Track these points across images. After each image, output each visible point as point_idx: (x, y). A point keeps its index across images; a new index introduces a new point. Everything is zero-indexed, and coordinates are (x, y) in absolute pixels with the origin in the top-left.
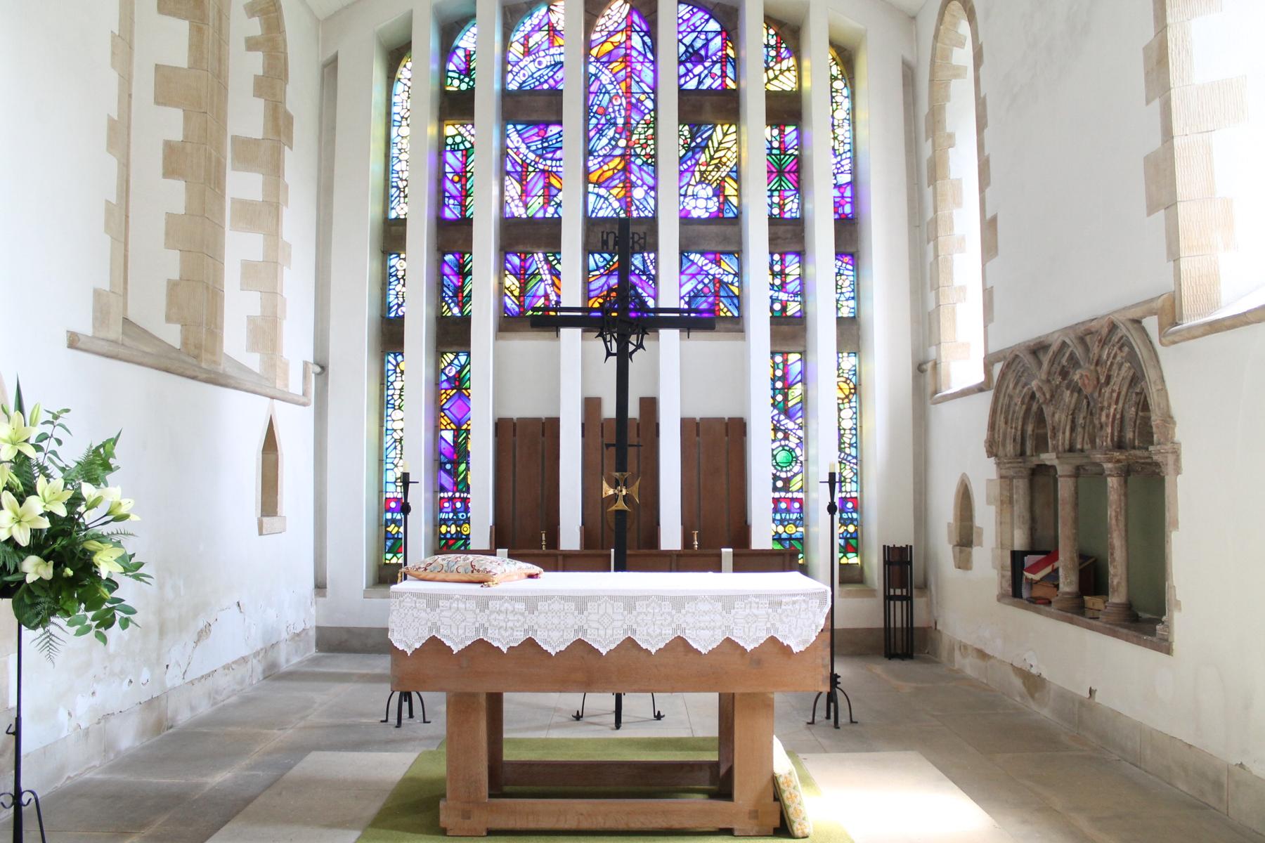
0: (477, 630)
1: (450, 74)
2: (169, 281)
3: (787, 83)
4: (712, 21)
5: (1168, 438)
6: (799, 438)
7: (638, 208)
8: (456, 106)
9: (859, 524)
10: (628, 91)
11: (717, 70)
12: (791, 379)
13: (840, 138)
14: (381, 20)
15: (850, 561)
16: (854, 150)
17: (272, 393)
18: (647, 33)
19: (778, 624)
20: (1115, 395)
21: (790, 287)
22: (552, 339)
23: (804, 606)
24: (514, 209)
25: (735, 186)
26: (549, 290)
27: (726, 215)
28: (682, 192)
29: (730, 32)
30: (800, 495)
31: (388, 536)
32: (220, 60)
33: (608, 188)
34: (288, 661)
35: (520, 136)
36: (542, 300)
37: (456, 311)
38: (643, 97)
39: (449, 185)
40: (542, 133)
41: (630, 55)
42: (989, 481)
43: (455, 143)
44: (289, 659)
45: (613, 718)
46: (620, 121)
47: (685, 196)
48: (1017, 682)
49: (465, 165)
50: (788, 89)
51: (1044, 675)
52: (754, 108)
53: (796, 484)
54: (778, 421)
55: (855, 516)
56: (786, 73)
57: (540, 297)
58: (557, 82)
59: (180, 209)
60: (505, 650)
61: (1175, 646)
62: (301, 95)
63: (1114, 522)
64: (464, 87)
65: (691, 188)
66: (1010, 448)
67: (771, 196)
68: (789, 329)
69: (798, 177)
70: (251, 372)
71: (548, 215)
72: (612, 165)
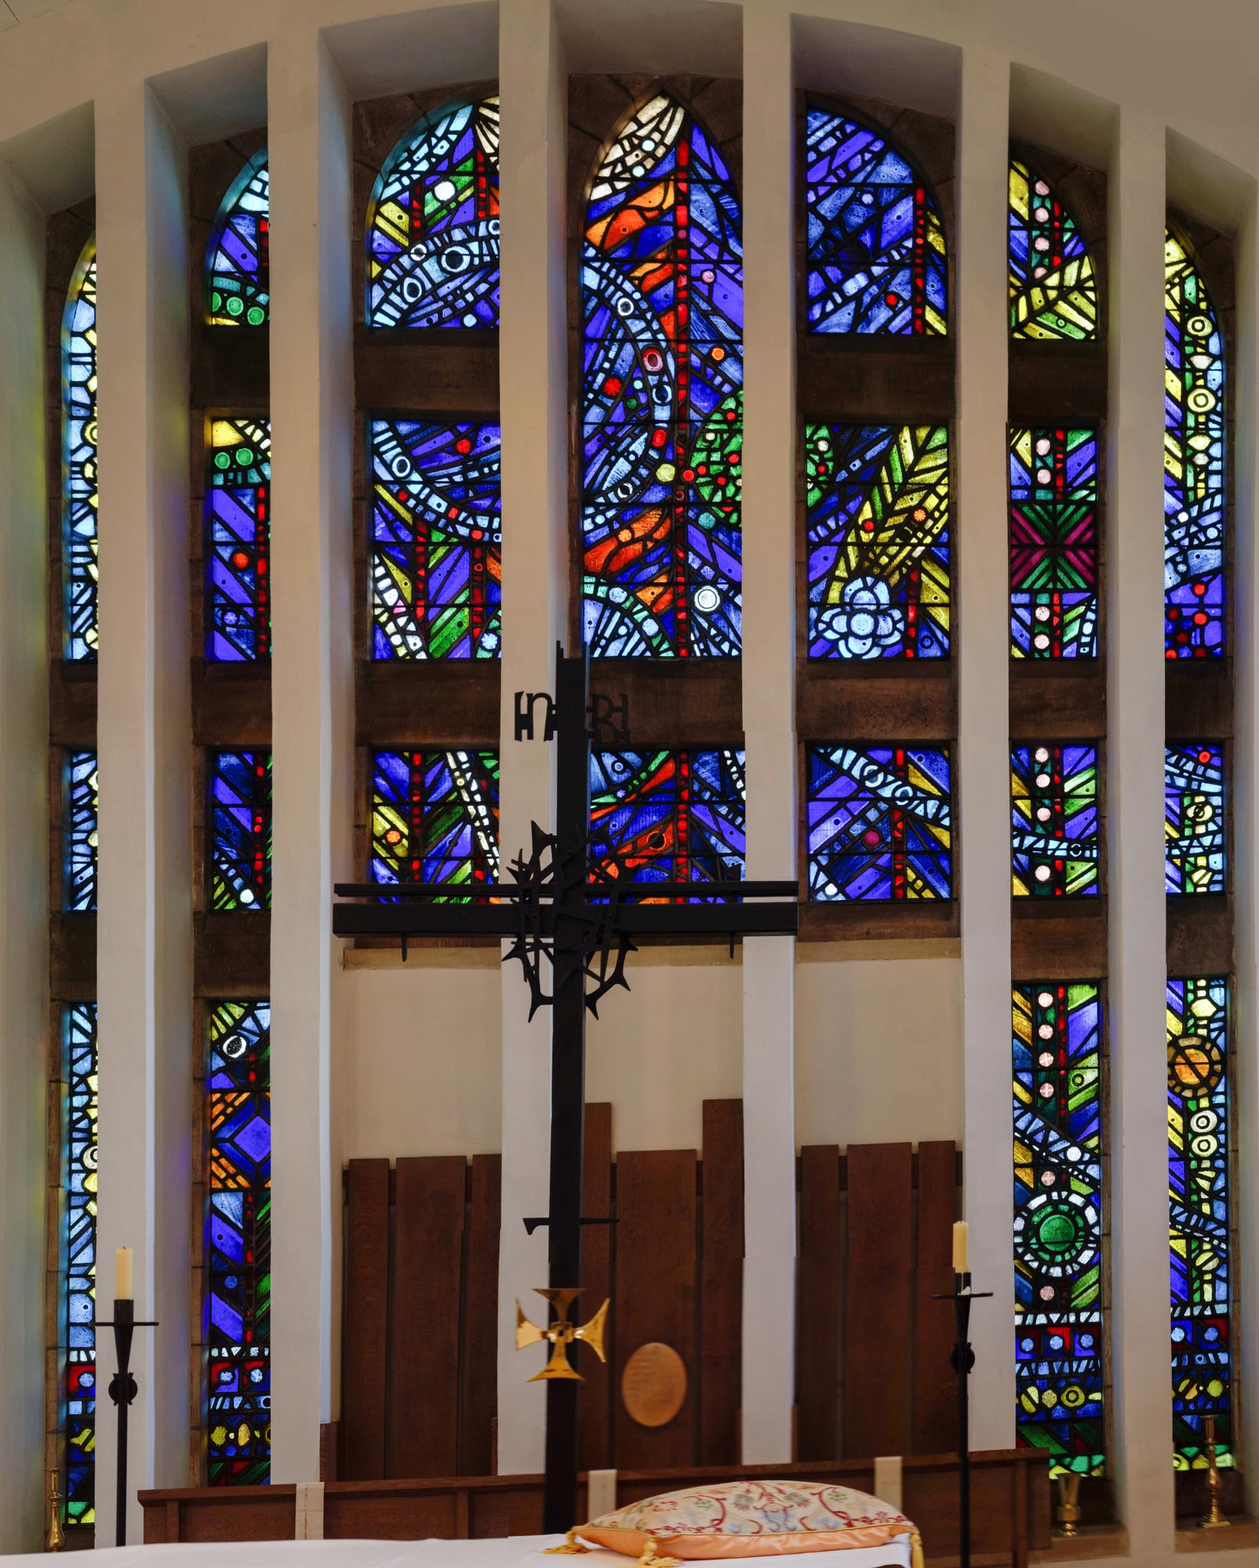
3: (1077, 319)
6: (1093, 1182)
11: (900, 285)
12: (1073, 1046)
13: (1201, 460)
21: (1073, 827)
22: (719, 961)
25: (945, 581)
28: (814, 594)
29: (935, 190)
33: (632, 587)
36: (467, 868)
39: (221, 574)
40: (464, 446)
43: (235, 467)
47: (823, 606)
54: (1046, 1145)
57: (462, 861)
68: (1060, 930)
72: (640, 529)
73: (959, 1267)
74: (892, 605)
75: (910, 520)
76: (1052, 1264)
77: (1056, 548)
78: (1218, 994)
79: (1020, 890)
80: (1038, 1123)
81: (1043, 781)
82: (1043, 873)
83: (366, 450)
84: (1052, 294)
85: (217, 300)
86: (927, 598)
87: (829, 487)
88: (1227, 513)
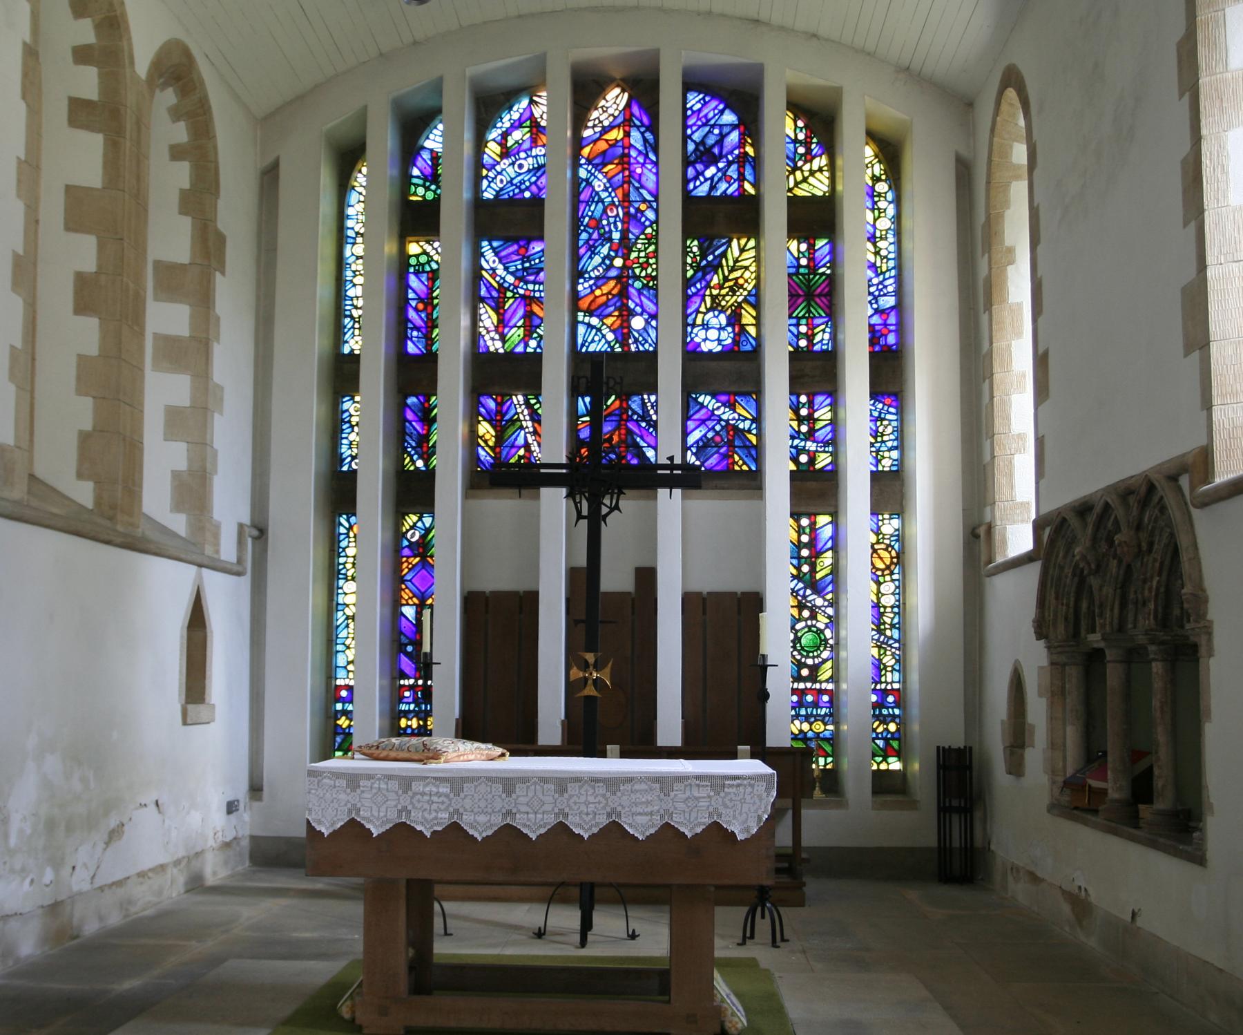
0: (400, 812)
1: (414, 181)
2: (81, 432)
3: (819, 186)
4: (727, 112)
5: (1201, 615)
6: (829, 617)
7: (636, 341)
8: (419, 219)
9: (902, 722)
10: (626, 199)
11: (733, 172)
12: (820, 545)
13: (883, 253)
14: (333, 117)
15: (891, 767)
16: (899, 267)
17: (199, 559)
18: (648, 129)
19: (721, 809)
20: (1157, 565)
23: (749, 789)
24: (489, 343)
26: (530, 439)
27: (744, 348)
29: (750, 125)
30: (830, 686)
31: (337, 730)
32: (138, 179)
33: (602, 317)
34: (215, 873)
35: (496, 254)
36: (522, 452)
37: (420, 464)
38: (643, 207)
39: (412, 314)
41: (629, 156)
42: (1040, 668)
44: (214, 870)
45: (577, 938)
46: (616, 236)
48: (1066, 908)
49: (431, 290)
50: (820, 194)
51: (1093, 898)
52: (775, 216)
53: (826, 672)
54: (804, 597)
55: (897, 712)
56: (818, 175)
57: (519, 448)
58: (540, 189)
59: (93, 349)
60: (428, 835)
61: (1209, 855)
62: (235, 212)
63: (1158, 714)
64: (430, 196)
65: (700, 316)
66: (1061, 628)
67: (797, 325)
68: (816, 489)
69: (830, 301)
70: (175, 535)
71: (529, 350)
72: (605, 289)
77: (809, 296)
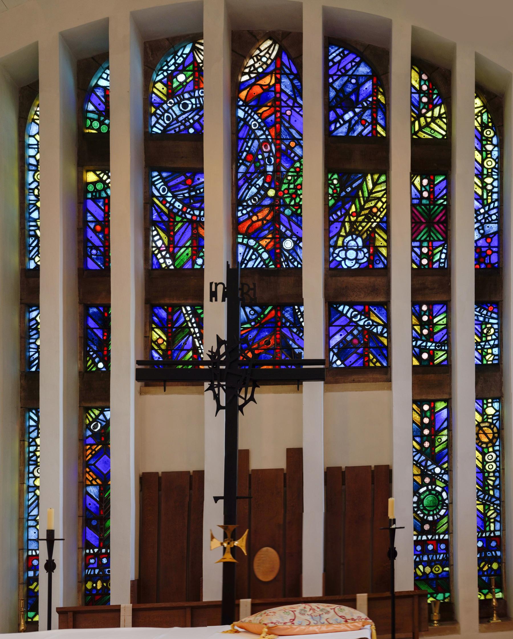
3: (439, 130)
6: (445, 482)
10: (278, 137)
11: (367, 116)
12: (437, 427)
13: (489, 187)
21: (437, 337)
22: (293, 392)
28: (332, 242)
29: (381, 77)
33: (257, 239)
36: (190, 354)
39: (90, 234)
40: (189, 182)
43: (96, 190)
47: (335, 247)
54: (426, 467)
57: (188, 351)
68: (432, 379)
72: (261, 216)
73: (391, 516)
74: (364, 247)
75: (371, 212)
76: (429, 515)
77: (430, 223)
78: (496, 405)
79: (416, 363)
80: (423, 458)
81: (425, 318)
82: (425, 356)
83: (149, 184)
84: (429, 120)
85: (88, 122)
86: (378, 244)
87: (338, 198)
88: (500, 209)
